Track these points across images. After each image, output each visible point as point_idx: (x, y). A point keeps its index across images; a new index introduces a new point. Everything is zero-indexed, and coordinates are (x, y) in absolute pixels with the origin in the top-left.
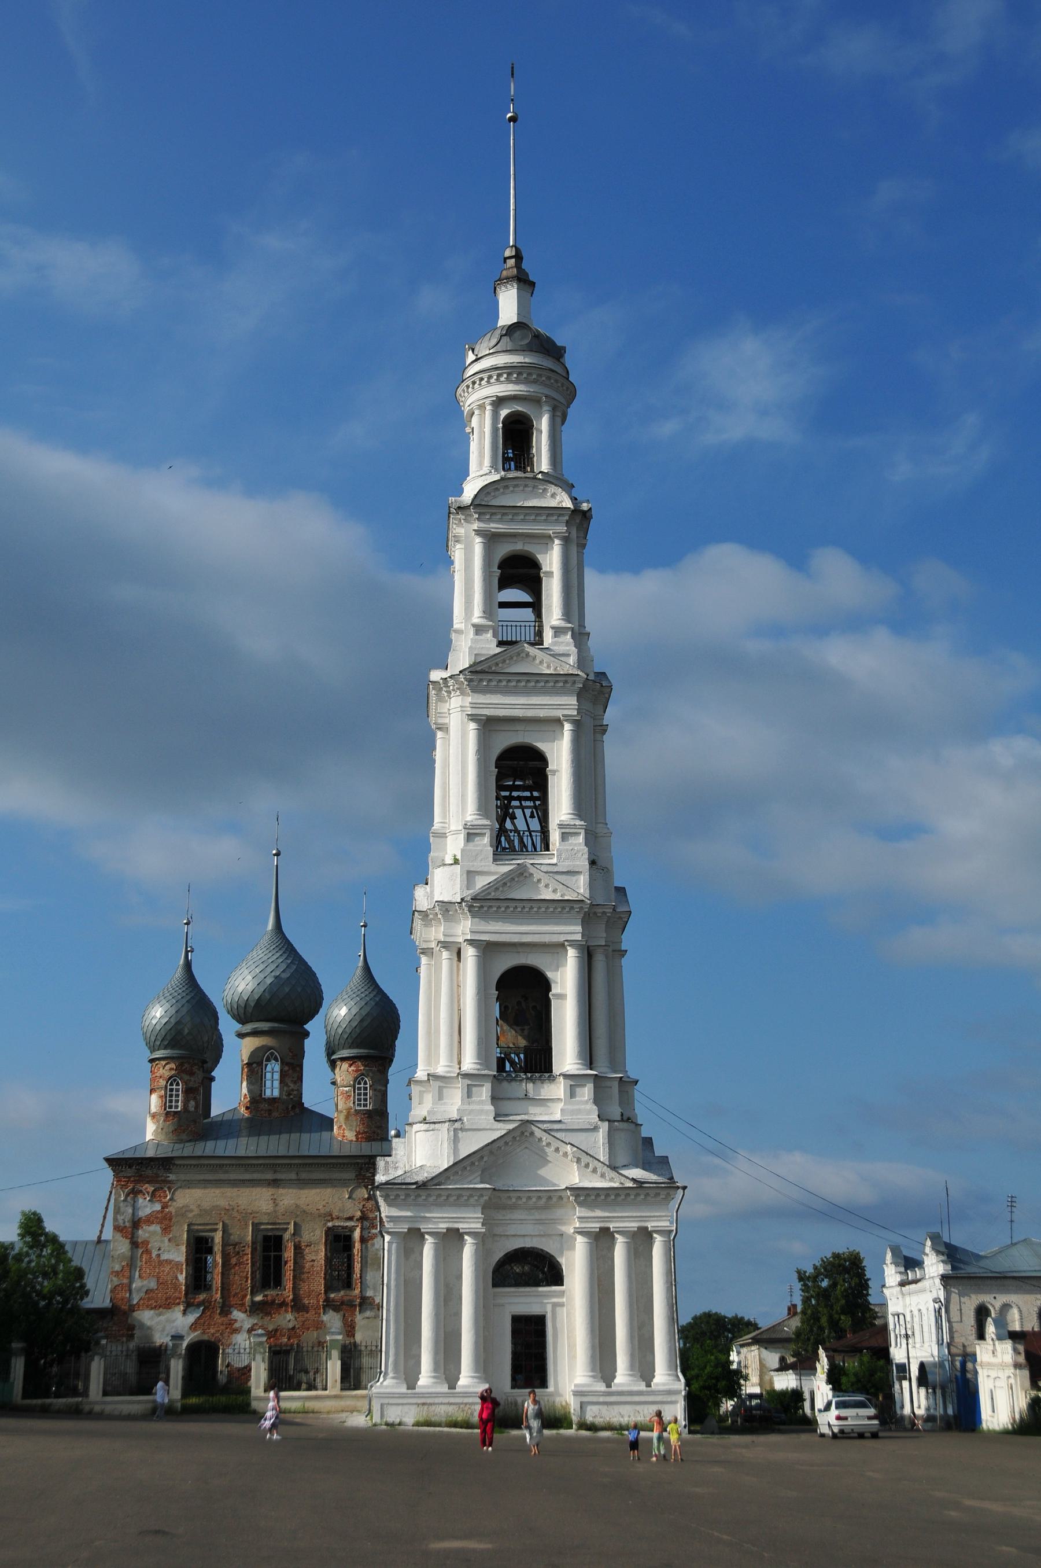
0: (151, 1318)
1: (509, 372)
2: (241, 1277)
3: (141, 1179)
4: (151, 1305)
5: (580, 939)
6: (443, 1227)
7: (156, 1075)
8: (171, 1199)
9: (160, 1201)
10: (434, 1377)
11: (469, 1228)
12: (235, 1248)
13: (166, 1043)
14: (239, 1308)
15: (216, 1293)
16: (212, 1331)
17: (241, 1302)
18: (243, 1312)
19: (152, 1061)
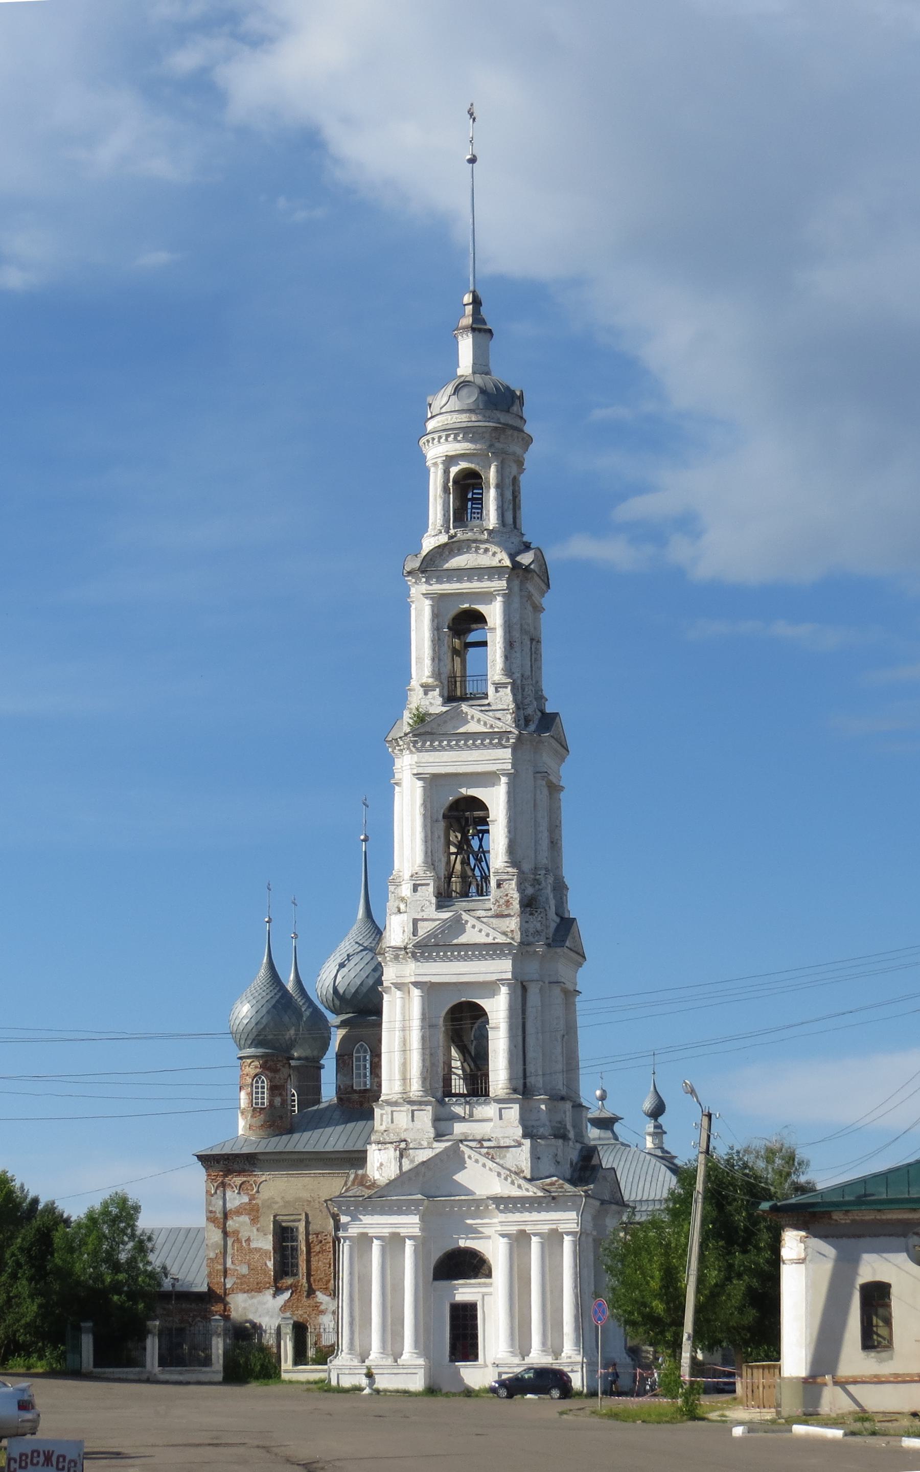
0: (245, 1301)
1: (466, 432)
2: (324, 1263)
3: (228, 1172)
4: (244, 1288)
5: (510, 977)
6: (385, 1231)
7: (244, 1072)
8: (258, 1192)
9: (248, 1194)
10: (511, 1352)
11: (407, 1233)
12: (317, 1237)
13: (249, 1042)
14: (324, 1292)
15: (303, 1279)
16: (300, 1312)
17: (325, 1287)
18: (327, 1296)
19: (241, 1058)
